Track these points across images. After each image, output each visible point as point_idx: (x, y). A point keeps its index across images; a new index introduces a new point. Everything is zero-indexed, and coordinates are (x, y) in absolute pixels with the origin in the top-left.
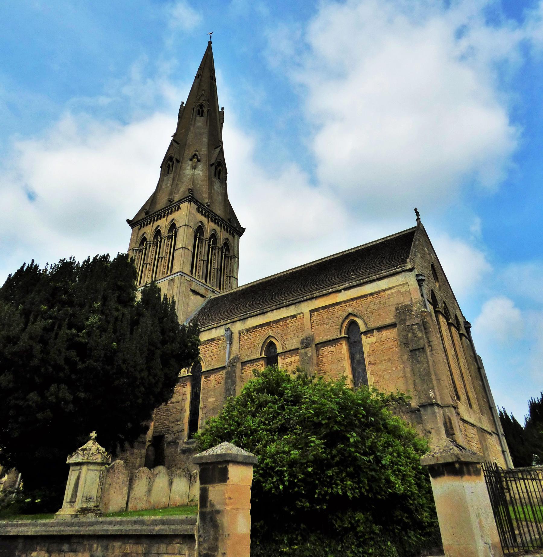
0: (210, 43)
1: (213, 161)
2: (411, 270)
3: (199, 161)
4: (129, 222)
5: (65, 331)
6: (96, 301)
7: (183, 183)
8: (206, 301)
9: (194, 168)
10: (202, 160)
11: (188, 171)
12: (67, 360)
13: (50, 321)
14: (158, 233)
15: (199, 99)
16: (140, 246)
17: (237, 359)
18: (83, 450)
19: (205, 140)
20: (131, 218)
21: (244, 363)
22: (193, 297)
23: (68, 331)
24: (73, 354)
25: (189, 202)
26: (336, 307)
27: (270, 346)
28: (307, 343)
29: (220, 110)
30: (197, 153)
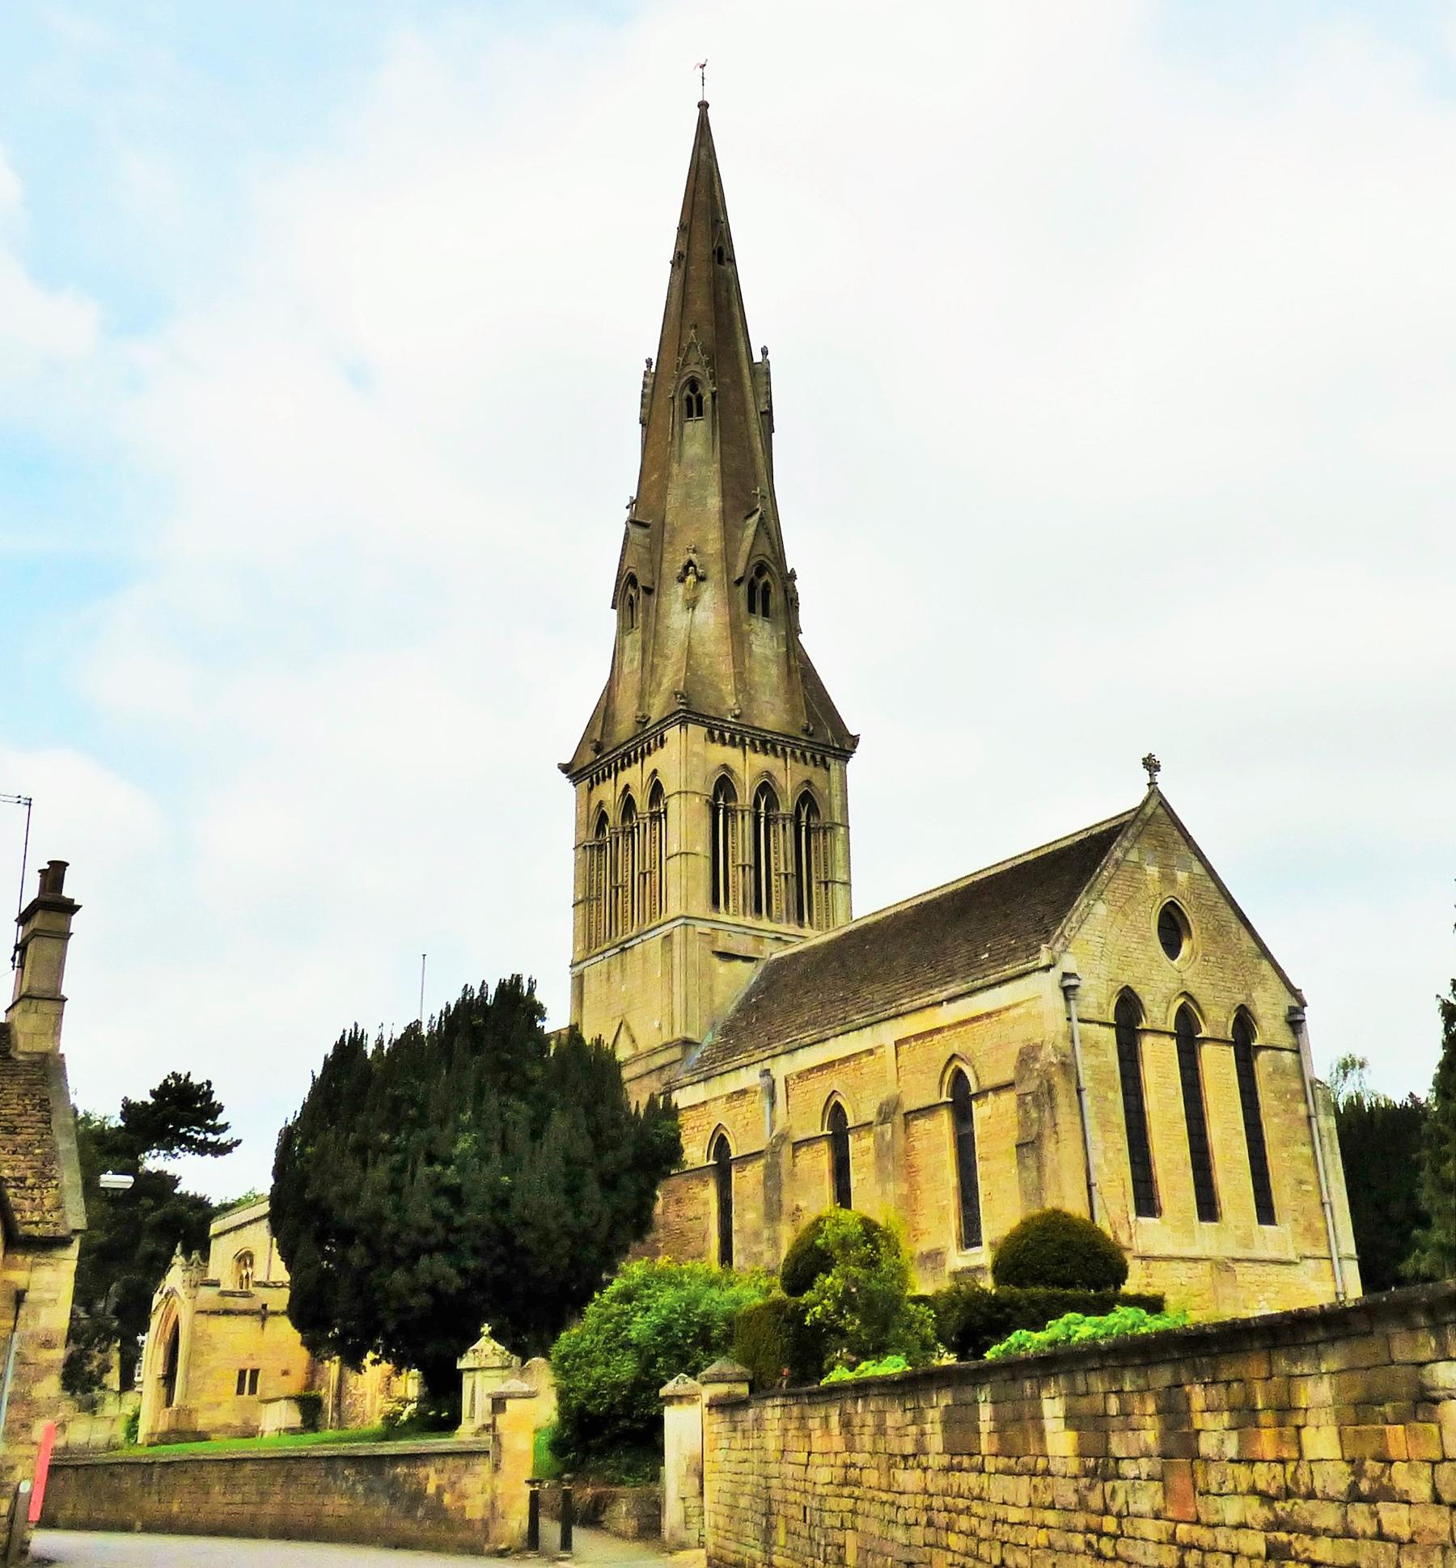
0: (703, 106)
1: (740, 570)
2: (1047, 968)
3: (701, 579)
4: (565, 768)
5: (423, 1170)
6: (462, 1110)
7: (667, 658)
8: (760, 968)
9: (692, 604)
10: (710, 574)
11: (677, 618)
12: (436, 1215)
13: (398, 1158)
14: (629, 805)
15: (685, 364)
16: (597, 834)
17: (783, 1137)
18: (475, 1351)
19: (714, 502)
20: (567, 761)
21: (797, 1146)
22: (722, 968)
23: (427, 1170)
24: (443, 1204)
25: (683, 723)
26: (937, 1037)
27: (836, 1114)
28: (887, 1112)
29: (757, 357)
30: (693, 557)
